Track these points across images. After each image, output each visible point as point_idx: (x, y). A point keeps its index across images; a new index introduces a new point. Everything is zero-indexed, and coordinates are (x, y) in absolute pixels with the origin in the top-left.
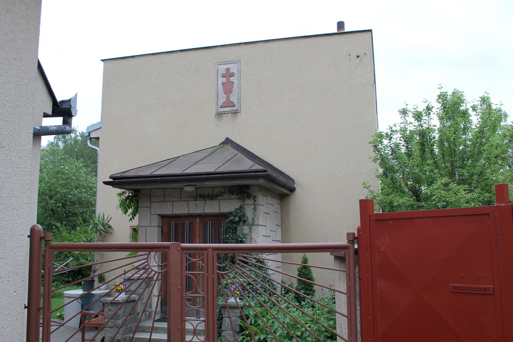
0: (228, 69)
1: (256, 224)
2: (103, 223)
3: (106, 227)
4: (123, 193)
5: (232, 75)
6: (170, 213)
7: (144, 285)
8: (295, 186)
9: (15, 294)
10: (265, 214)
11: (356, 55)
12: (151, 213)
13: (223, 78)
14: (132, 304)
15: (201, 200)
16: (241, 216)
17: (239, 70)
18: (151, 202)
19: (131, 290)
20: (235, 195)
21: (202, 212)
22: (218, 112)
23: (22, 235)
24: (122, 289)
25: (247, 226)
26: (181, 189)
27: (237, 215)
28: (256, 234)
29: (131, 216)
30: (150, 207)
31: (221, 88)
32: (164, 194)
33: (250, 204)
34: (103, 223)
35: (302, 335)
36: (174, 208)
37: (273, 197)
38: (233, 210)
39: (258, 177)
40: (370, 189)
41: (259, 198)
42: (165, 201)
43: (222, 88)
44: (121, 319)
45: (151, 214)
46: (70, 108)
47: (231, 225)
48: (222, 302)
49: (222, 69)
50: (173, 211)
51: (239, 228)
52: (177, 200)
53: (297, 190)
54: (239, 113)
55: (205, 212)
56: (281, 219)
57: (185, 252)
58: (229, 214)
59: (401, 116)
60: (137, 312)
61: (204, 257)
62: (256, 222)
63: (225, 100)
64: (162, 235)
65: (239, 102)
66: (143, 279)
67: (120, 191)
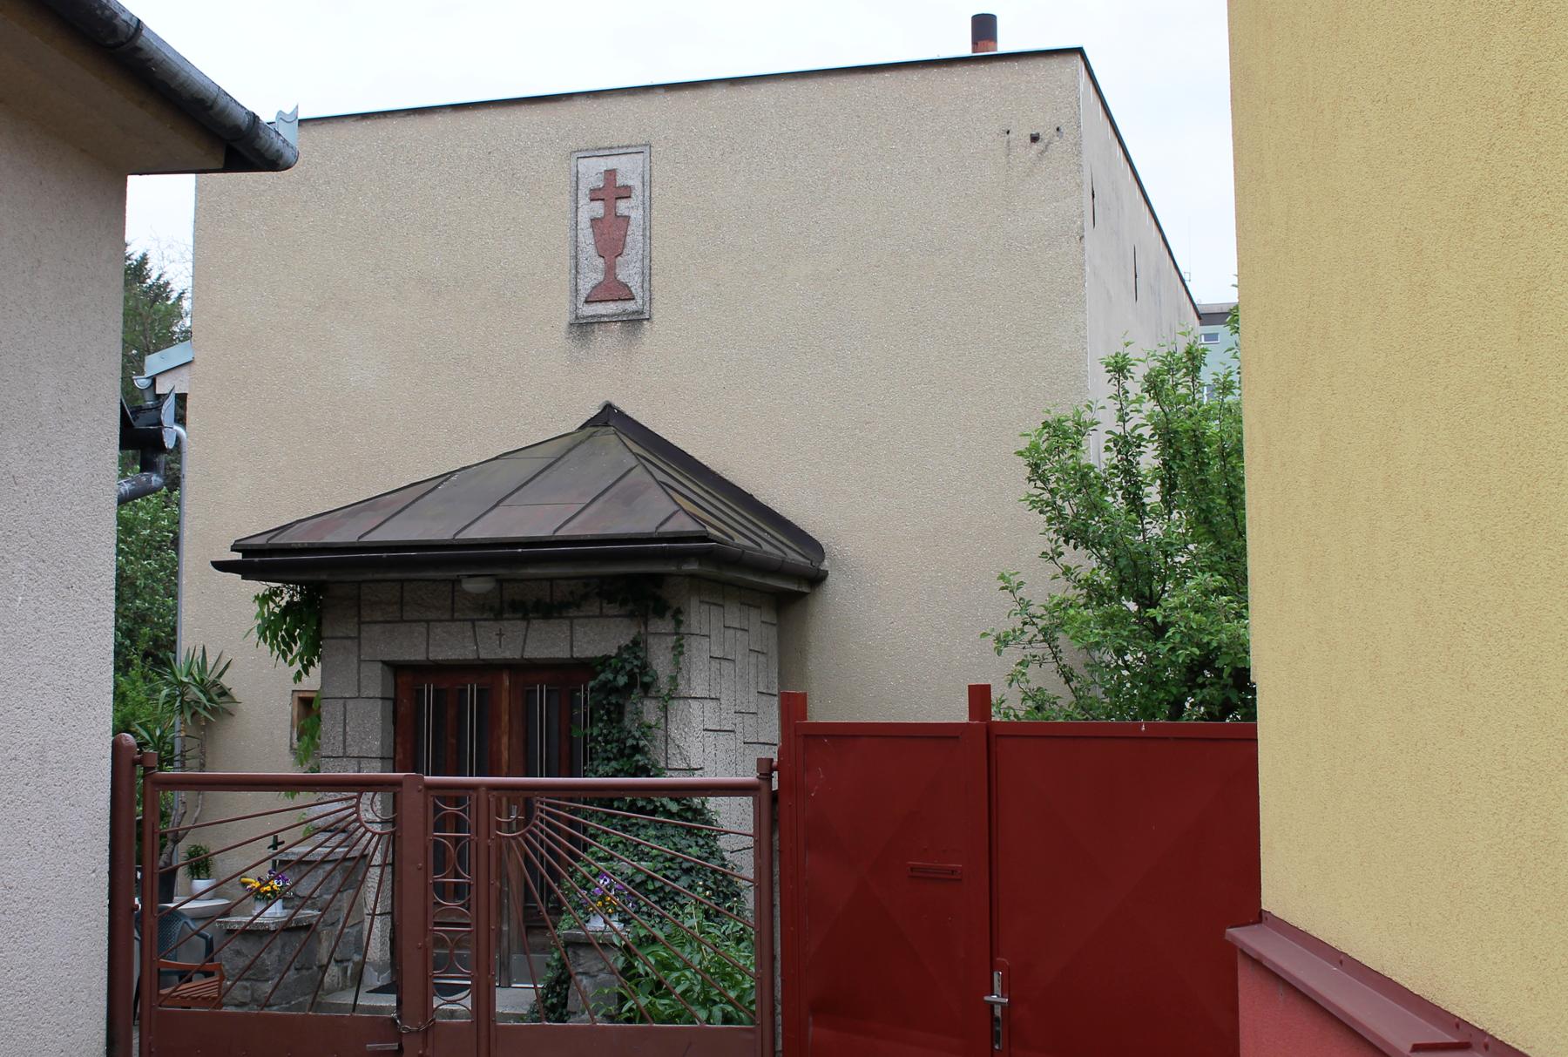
0: (611, 174)
1: (682, 695)
2: (202, 680)
3: (214, 692)
4: (275, 593)
5: (625, 193)
6: (418, 658)
7: (338, 879)
8: (826, 565)
9: (93, 875)
10: (715, 664)
11: (1027, 132)
12: (359, 656)
13: (593, 203)
14: (304, 936)
15: (513, 619)
16: (636, 670)
17: (647, 177)
18: (360, 623)
19: (299, 893)
20: (618, 604)
21: (517, 656)
22: (577, 318)
23: (104, 757)
24: (273, 892)
25: (653, 702)
26: (458, 581)
27: (623, 668)
28: (681, 726)
29: (298, 666)
30: (359, 638)
31: (586, 236)
32: (402, 597)
33: (665, 634)
34: (202, 680)
35: (739, 998)
36: (431, 642)
37: (750, 605)
38: (614, 652)
39: (684, 556)
40: (1019, 594)
41: (692, 615)
42: (402, 621)
43: (592, 236)
44: (273, 979)
45: (360, 661)
46: (160, 430)
47: (604, 699)
48: (570, 928)
49: (592, 171)
50: (428, 653)
51: (629, 708)
52: (443, 618)
53: (830, 579)
54: (645, 322)
55: (527, 655)
56: (779, 673)
57: (432, 793)
58: (601, 664)
59: (1109, 376)
60: (319, 961)
61: (435, 816)
62: (683, 689)
63: (601, 277)
64: (395, 723)
65: (646, 285)
66: (336, 860)
67: (261, 587)
